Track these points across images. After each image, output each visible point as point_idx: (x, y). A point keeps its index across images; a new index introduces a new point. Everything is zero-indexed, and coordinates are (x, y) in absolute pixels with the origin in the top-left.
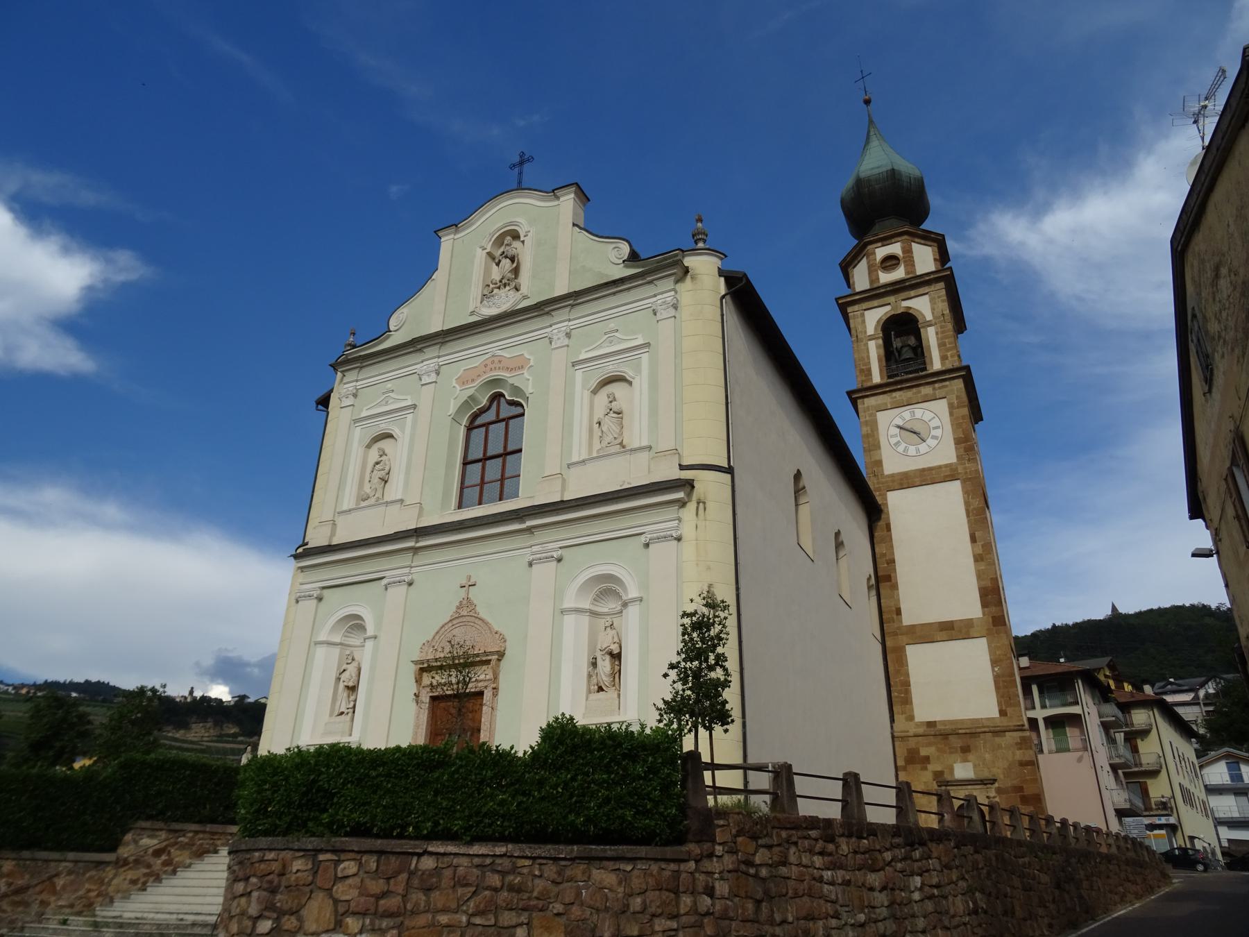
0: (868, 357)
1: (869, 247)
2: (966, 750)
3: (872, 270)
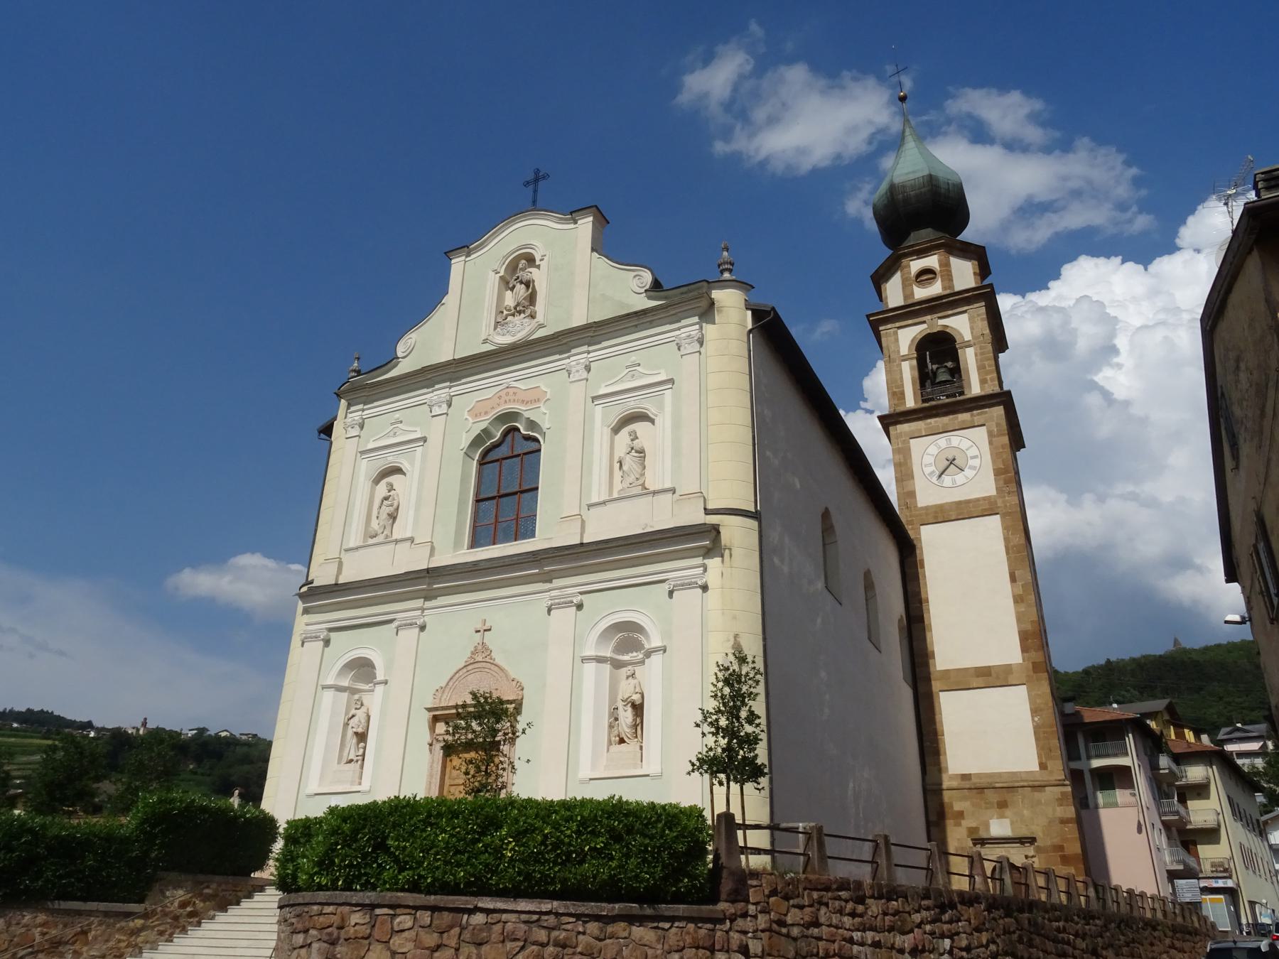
0: (902, 378)
1: (904, 261)
2: (1003, 805)
3: (906, 284)
